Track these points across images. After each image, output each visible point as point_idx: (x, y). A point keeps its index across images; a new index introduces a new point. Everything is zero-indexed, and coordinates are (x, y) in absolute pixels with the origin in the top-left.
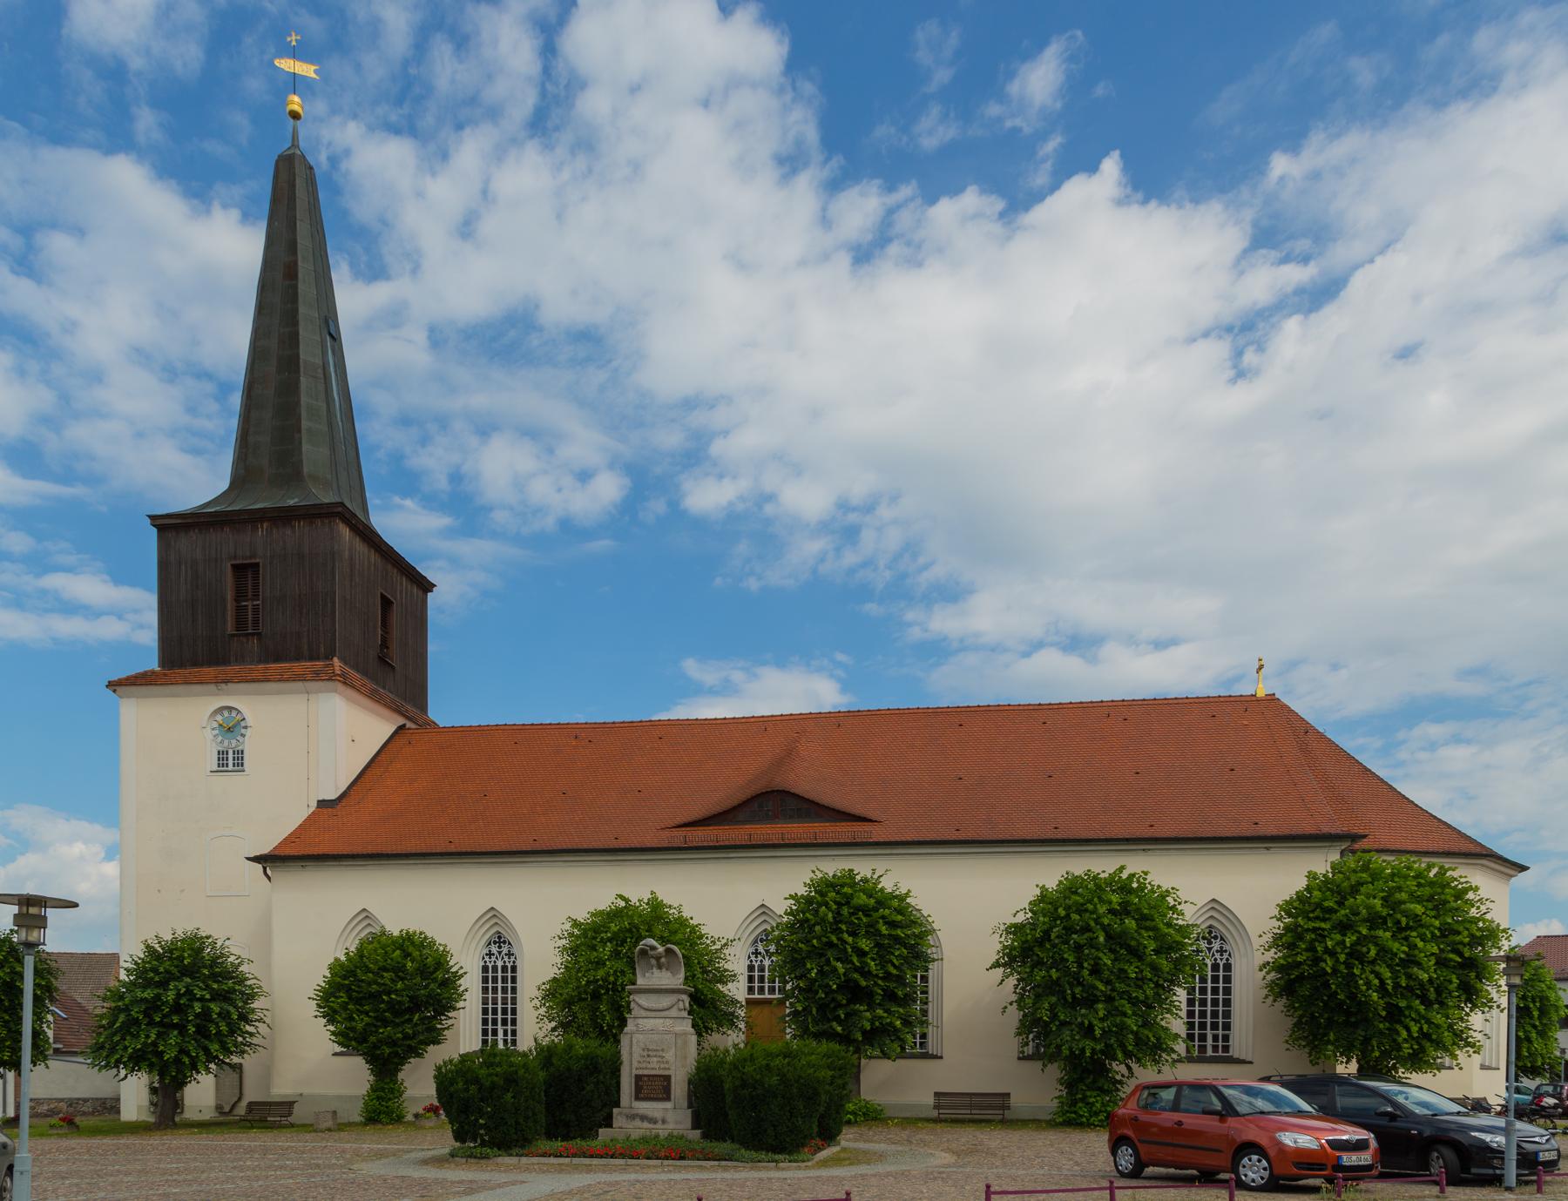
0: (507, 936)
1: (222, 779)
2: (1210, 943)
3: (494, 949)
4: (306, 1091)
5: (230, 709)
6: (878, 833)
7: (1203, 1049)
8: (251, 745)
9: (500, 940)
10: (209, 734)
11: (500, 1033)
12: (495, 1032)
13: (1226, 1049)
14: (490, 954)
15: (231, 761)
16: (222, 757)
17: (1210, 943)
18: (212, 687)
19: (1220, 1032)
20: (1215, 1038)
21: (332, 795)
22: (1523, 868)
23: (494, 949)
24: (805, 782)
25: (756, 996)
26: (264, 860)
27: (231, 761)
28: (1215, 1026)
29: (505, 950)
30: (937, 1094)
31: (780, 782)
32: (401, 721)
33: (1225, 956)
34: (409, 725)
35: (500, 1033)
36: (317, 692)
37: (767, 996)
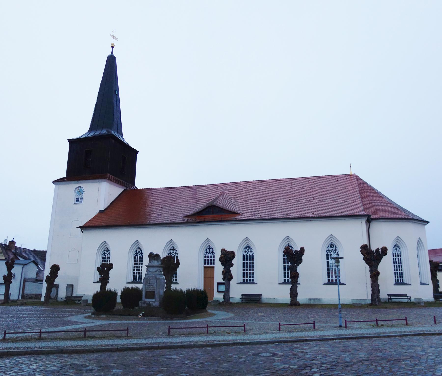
0: (251, 245)
1: (77, 205)
2: (332, 248)
3: (246, 250)
4: (86, 293)
5: (80, 187)
6: (239, 217)
7: (247, 280)
8: (84, 197)
9: (248, 247)
10: (74, 194)
11: (138, 276)
12: (136, 276)
13: (253, 280)
14: (136, 253)
15: (79, 200)
16: (77, 199)
17: (332, 248)
18: (76, 182)
19: (251, 275)
20: (250, 277)
21: (103, 209)
22: (428, 222)
23: (246, 250)
24: (220, 203)
25: (207, 265)
26: (83, 228)
27: (79, 200)
28: (250, 273)
29: (211, 251)
30: (242, 295)
31: (215, 203)
32: (125, 188)
33: (337, 251)
34: (128, 189)
35: (138, 276)
36: (102, 182)
37: (209, 265)
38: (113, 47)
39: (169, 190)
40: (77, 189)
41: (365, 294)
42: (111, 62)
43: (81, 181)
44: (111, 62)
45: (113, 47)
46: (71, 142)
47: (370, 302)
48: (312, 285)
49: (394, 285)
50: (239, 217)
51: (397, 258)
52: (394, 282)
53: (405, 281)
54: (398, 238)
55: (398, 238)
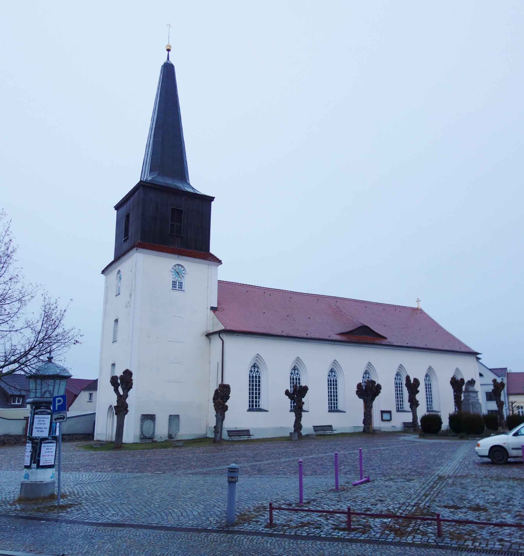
5: (182, 266)
6: (384, 342)
8: (186, 282)
15: (177, 286)
16: (174, 283)
18: (176, 256)
38: (169, 50)
39: (338, 300)
40: (177, 267)
41: (359, 422)
42: (168, 72)
43: (184, 257)
44: (168, 72)
45: (169, 50)
46: (208, 200)
47: (361, 430)
48: (316, 413)
49: (248, 411)
50: (384, 342)
51: (428, 387)
52: (248, 408)
53: (340, 408)
54: (258, 356)
55: (258, 356)
